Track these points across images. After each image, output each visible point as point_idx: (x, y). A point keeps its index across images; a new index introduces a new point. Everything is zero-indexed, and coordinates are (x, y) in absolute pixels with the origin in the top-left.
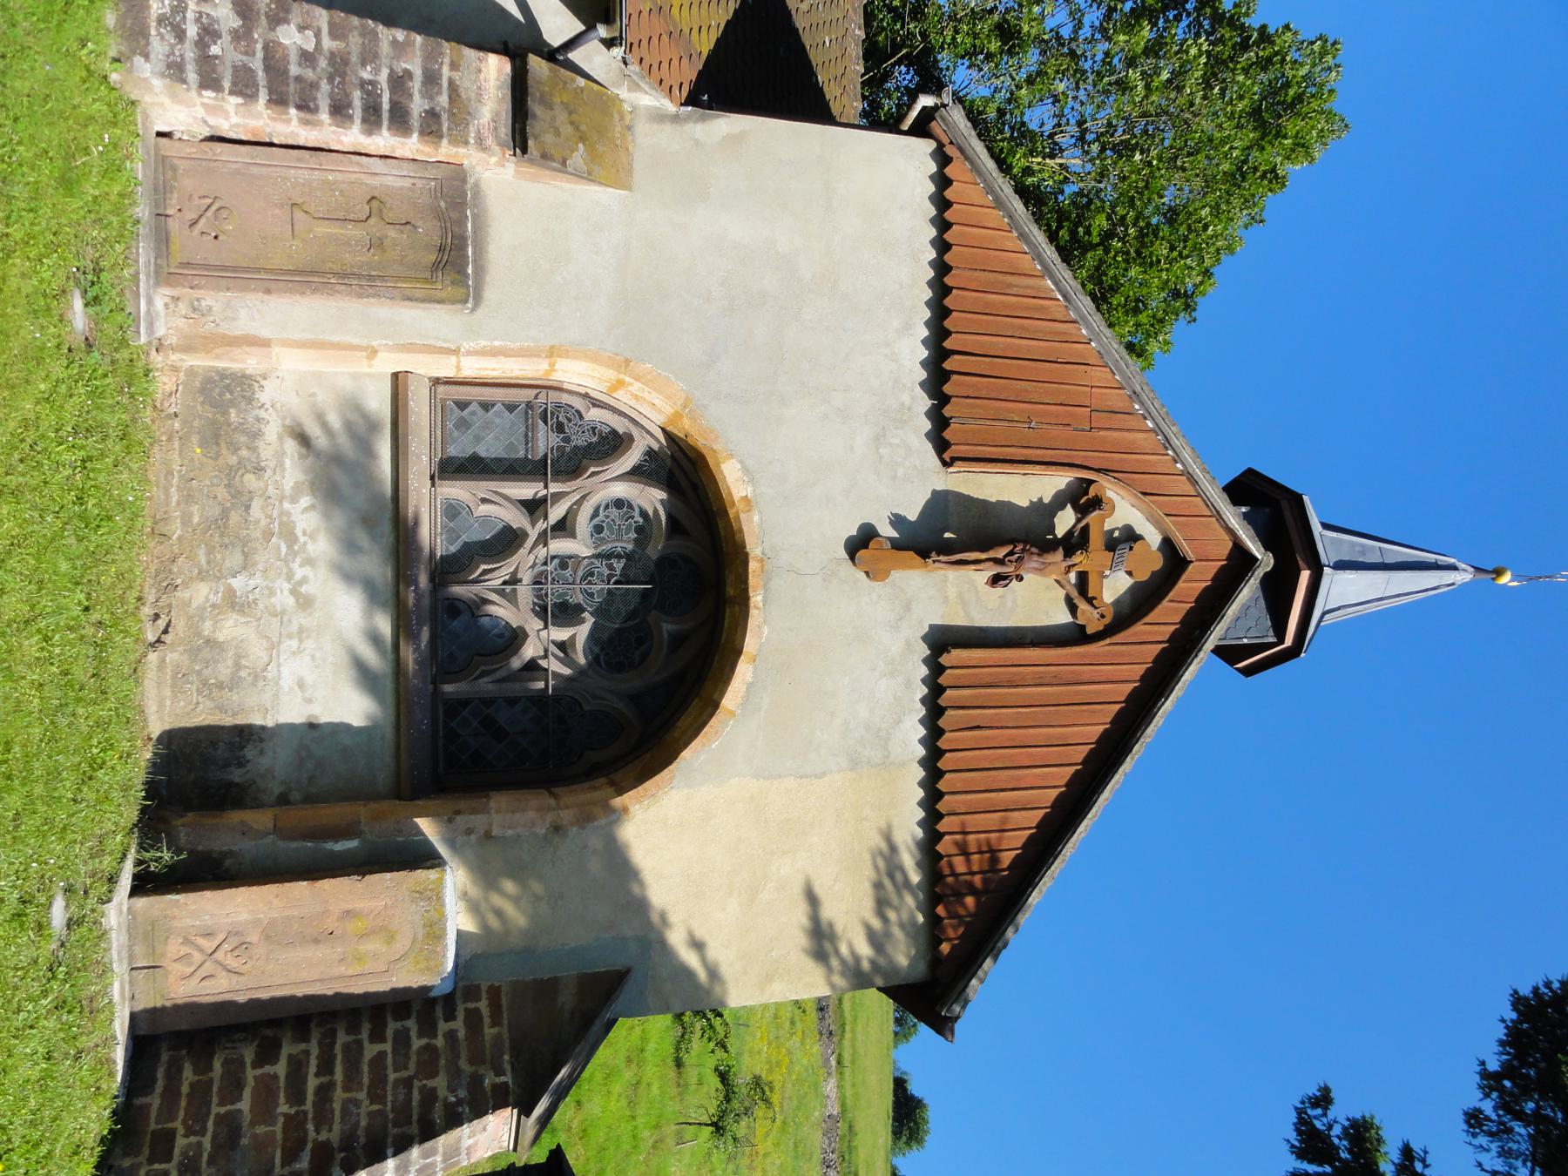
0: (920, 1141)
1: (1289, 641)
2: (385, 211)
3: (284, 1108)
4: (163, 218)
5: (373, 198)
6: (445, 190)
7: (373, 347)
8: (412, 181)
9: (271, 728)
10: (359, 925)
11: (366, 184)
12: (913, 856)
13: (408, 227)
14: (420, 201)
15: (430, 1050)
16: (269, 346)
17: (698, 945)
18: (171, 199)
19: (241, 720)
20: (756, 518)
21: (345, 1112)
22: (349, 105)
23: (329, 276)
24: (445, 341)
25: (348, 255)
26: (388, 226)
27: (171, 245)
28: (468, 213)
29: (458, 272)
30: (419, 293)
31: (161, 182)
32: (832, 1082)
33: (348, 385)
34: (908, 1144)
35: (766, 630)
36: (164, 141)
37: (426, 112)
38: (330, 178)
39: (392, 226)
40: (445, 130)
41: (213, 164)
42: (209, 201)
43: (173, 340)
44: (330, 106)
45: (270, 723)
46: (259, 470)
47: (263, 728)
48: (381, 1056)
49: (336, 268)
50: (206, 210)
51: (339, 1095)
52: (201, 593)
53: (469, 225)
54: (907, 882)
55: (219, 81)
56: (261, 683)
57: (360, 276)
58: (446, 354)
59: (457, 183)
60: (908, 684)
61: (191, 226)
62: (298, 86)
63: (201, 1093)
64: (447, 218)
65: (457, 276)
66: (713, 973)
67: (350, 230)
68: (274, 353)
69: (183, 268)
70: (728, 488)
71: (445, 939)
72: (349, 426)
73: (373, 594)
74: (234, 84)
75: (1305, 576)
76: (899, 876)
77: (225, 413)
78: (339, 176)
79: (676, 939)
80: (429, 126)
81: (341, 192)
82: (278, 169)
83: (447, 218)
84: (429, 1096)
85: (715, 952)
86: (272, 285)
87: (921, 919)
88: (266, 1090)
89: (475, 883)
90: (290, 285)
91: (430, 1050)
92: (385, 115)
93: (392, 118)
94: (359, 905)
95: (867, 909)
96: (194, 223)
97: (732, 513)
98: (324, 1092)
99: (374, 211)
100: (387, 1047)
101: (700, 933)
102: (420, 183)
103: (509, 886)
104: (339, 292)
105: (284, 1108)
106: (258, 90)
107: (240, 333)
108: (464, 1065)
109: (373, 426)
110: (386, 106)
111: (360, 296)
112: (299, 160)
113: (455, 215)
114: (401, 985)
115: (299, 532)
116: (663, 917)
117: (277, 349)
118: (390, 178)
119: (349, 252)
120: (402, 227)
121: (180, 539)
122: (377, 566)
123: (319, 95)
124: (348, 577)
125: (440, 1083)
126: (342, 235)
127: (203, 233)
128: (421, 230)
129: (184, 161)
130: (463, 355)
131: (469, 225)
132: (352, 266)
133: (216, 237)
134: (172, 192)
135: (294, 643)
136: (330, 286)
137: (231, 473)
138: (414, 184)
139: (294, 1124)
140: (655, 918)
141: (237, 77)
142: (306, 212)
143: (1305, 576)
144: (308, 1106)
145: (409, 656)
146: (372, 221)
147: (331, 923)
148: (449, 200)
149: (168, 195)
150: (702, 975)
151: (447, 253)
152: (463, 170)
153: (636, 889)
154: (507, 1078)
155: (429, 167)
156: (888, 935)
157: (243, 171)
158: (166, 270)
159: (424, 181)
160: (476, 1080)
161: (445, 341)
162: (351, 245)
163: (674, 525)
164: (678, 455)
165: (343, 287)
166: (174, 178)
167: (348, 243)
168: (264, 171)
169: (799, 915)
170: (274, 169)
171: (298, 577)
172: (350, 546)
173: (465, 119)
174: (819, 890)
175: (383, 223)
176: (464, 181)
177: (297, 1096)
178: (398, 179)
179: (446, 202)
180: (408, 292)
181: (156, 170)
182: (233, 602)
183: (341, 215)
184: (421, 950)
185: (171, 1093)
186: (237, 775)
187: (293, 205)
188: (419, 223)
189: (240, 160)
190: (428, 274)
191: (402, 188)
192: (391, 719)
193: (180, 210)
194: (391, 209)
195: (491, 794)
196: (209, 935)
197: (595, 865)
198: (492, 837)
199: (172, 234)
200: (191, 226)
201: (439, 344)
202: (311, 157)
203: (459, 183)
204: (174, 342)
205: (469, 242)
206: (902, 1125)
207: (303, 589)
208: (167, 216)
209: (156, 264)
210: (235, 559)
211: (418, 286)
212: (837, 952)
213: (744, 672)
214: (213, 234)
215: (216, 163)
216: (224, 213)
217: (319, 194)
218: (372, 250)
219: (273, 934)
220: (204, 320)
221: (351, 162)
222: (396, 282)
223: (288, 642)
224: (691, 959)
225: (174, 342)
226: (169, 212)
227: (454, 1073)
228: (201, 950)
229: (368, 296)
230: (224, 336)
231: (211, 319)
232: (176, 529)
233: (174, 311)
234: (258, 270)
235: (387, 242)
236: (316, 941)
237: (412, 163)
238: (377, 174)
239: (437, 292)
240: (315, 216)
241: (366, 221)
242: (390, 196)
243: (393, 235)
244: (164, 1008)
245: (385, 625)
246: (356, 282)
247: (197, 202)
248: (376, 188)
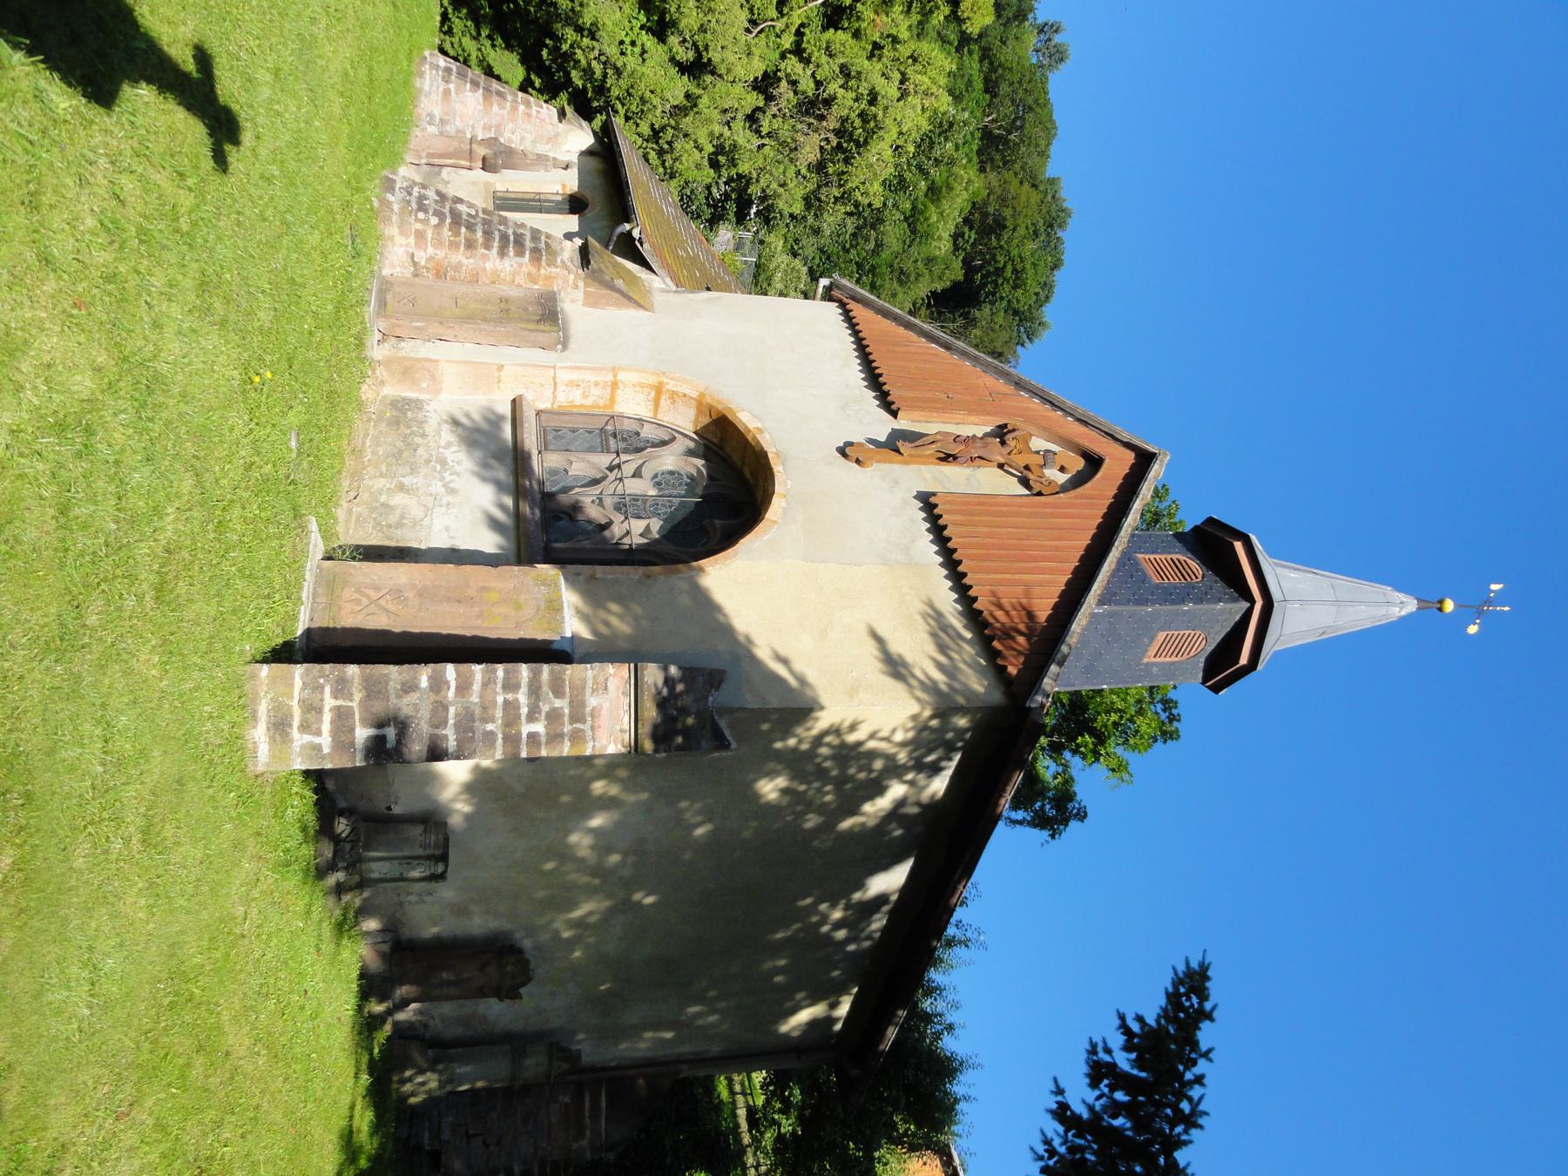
1: (1244, 659)
9: (425, 550)
10: (494, 596)
12: (959, 621)
17: (784, 661)
19: (401, 544)
20: (768, 436)
33: (485, 404)
35: (789, 482)
45: (423, 547)
46: (424, 436)
47: (419, 550)
54: (961, 637)
56: (418, 527)
66: (802, 681)
70: (744, 424)
71: (562, 612)
72: (486, 419)
73: (500, 486)
76: (951, 631)
77: (405, 414)
79: (763, 653)
85: (798, 666)
87: (983, 662)
89: (585, 603)
94: (494, 584)
95: (931, 649)
97: (749, 438)
101: (783, 652)
103: (614, 607)
109: (501, 418)
114: (528, 637)
115: (449, 461)
116: (748, 638)
121: (369, 460)
124: (484, 479)
135: (444, 510)
140: (741, 639)
147: (470, 592)
150: (793, 682)
153: (721, 618)
156: (956, 668)
163: (711, 477)
164: (706, 442)
169: (871, 648)
171: (447, 480)
172: (485, 465)
174: (883, 632)
182: (402, 488)
184: (544, 616)
192: (513, 547)
196: (376, 588)
197: (685, 600)
198: (595, 578)
207: (451, 485)
212: (914, 676)
223: (439, 509)
224: (781, 670)
228: (368, 597)
232: (368, 455)
236: (459, 601)
244: (334, 629)
245: (509, 501)
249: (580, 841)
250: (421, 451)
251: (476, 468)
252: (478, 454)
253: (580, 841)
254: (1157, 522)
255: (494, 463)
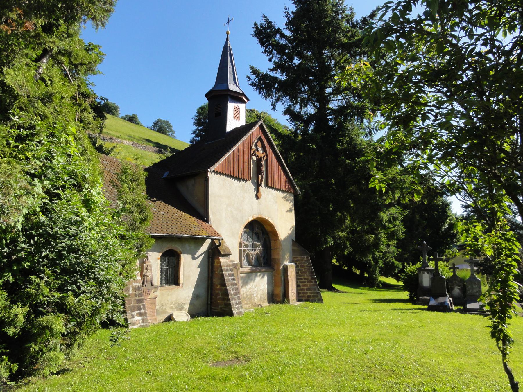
0: (117, 107)
3: (306, 283)
15: (301, 266)
21: (307, 276)
32: (124, 141)
34: (117, 111)
46: (244, 294)
48: (301, 272)
51: (306, 277)
52: (256, 300)
60: (269, 192)
63: (304, 293)
73: (256, 276)
75: (243, 97)
84: (307, 266)
85: (291, 227)
88: (304, 286)
91: (301, 266)
98: (305, 279)
100: (300, 271)
105: (306, 283)
108: (303, 262)
122: (254, 274)
124: (255, 279)
125: (305, 265)
137: (244, 298)
139: (308, 282)
143: (243, 97)
144: (306, 281)
145: (263, 270)
154: (306, 257)
160: (306, 261)
169: (288, 213)
172: (251, 280)
177: (305, 282)
182: (257, 296)
185: (303, 297)
186: (271, 293)
195: (272, 257)
206: (111, 111)
210: (252, 296)
213: (270, 220)
219: (292, 287)
224: (291, 230)
227: (304, 263)
245: (259, 274)
249: (307, 23)
250: (248, 294)
251: (253, 282)
252: (249, 282)
253: (307, 23)
254: (393, 371)
255: (251, 277)
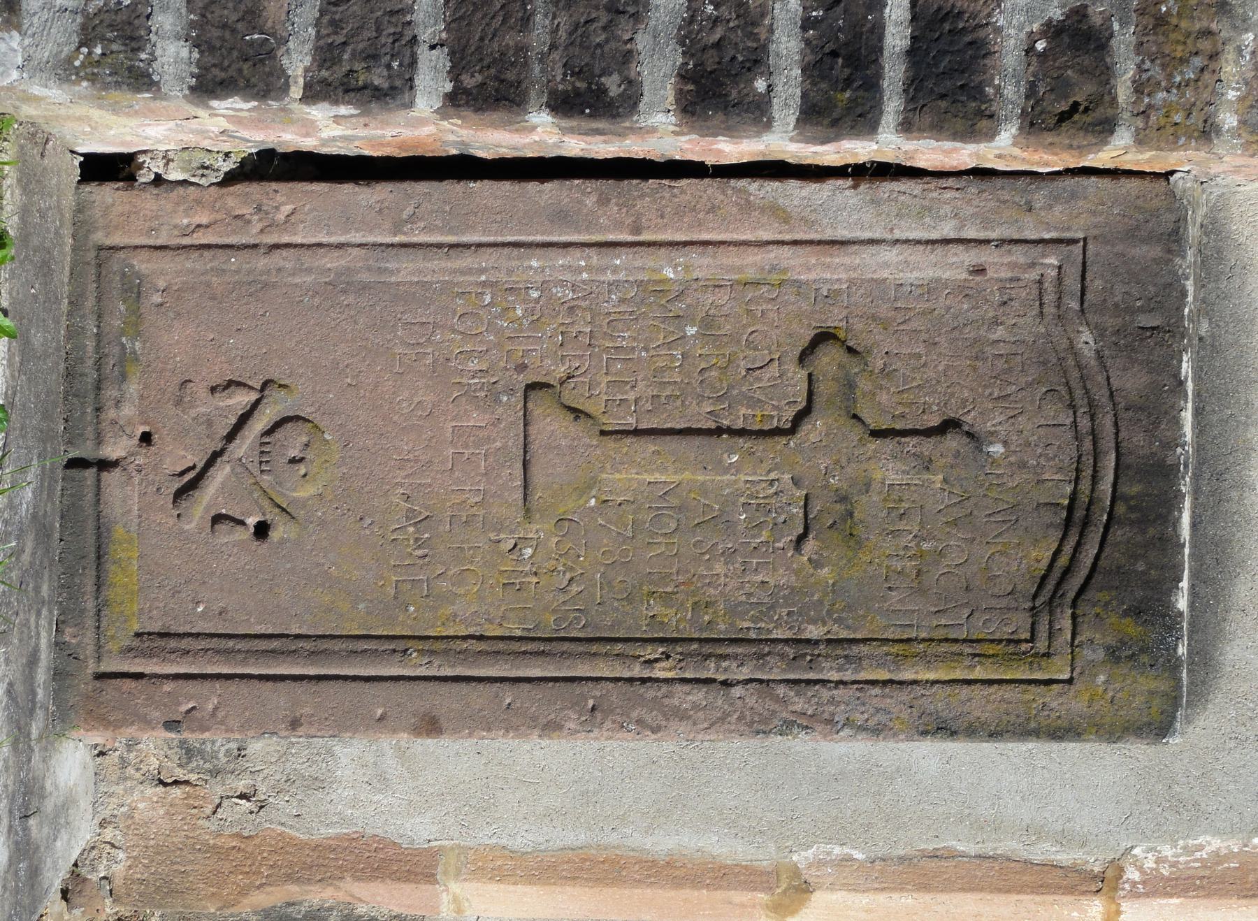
2: (864, 384)
4: (90, 473)
5: (823, 337)
6: (1095, 284)
7: (795, 872)
8: (970, 257)
11: (798, 284)
13: (952, 442)
14: (1000, 332)
16: (430, 878)
18: (118, 403)
22: (757, 61)
23: (650, 652)
24: (1063, 839)
25: (719, 568)
26: (874, 445)
27: (115, 575)
28: (1186, 368)
29: (1136, 612)
30: (981, 703)
31: (90, 345)
36: (106, 194)
37: (1053, 31)
38: (669, 273)
39: (889, 445)
40: (1123, 92)
41: (262, 262)
42: (243, 399)
43: (118, 866)
44: (683, 76)
49: (676, 620)
50: (231, 437)
53: (1187, 416)
55: (271, 54)
57: (760, 646)
58: (1070, 890)
59: (1147, 252)
61: (180, 494)
62: (563, 18)
64: (1101, 395)
65: (1131, 628)
67: (737, 468)
68: (445, 898)
69: (150, 654)
74: (326, 55)
78: (703, 265)
80: (1060, 86)
81: (708, 323)
82: (486, 259)
83: (1101, 395)
86: (445, 700)
90: (507, 695)
92: (894, 73)
93: (915, 89)
96: (190, 485)
99: (825, 389)
102: (998, 263)
104: (682, 716)
106: (413, 63)
107: (332, 831)
110: (897, 37)
111: (759, 727)
112: (561, 217)
113: (1131, 382)
117: (455, 887)
118: (890, 255)
119: (729, 555)
120: (927, 446)
123: (642, 42)
126: (703, 489)
127: (218, 519)
128: (997, 449)
129: (168, 263)
130: (1134, 895)
131: (1187, 416)
132: (734, 611)
133: (262, 530)
134: (123, 377)
136: (650, 692)
138: (979, 270)
141: (336, 25)
142: (577, 413)
146: (815, 428)
148: (1111, 322)
149: (110, 392)
151: (1095, 536)
152: (1171, 194)
155: (1040, 196)
157: (365, 277)
158: (91, 667)
159: (1019, 255)
161: (1063, 839)
162: (730, 525)
165: (698, 695)
166: (135, 323)
167: (722, 523)
168: (437, 268)
170: (467, 260)
173: (1207, 33)
175: (856, 432)
176: (1174, 238)
178: (918, 255)
179: (1100, 332)
180: (940, 702)
181: (75, 304)
183: (699, 414)
187: (532, 387)
188: (994, 421)
189: (356, 238)
190: (1018, 624)
191: (931, 288)
193: (146, 438)
194: (886, 373)
199: (119, 532)
200: (180, 494)
201: (1045, 852)
202: (603, 201)
203: (1156, 251)
204: (119, 869)
205: (1186, 487)
208: (105, 465)
209: (58, 645)
211: (978, 673)
214: (252, 521)
215: (278, 258)
216: (293, 441)
217: (624, 338)
218: (810, 545)
220: (217, 789)
221: (747, 206)
222: (900, 659)
225: (119, 869)
226: (112, 451)
229: (787, 727)
230: (284, 845)
231: (242, 785)
233: (124, 763)
234: (399, 644)
235: (869, 506)
237: (973, 187)
238: (843, 243)
239: (1051, 697)
240: (612, 423)
241: (792, 431)
242: (885, 324)
243: (893, 477)
246: (745, 673)
247: (205, 405)
248: (833, 295)
